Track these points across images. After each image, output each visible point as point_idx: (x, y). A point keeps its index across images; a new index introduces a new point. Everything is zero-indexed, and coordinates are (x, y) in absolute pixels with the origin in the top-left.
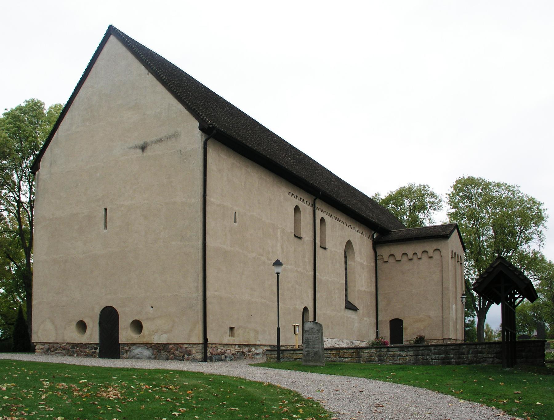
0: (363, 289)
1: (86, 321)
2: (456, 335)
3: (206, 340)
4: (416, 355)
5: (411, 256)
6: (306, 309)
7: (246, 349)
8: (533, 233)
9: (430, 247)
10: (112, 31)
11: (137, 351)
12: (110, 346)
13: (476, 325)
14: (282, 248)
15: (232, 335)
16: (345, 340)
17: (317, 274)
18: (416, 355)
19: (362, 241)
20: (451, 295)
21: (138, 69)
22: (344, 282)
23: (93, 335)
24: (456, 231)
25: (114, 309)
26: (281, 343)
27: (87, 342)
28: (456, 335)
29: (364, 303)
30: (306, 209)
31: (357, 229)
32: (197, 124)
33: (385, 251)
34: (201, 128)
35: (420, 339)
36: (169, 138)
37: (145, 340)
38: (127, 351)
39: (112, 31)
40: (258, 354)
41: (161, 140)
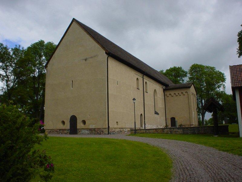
0: (160, 106)
1: (65, 121)
2: (195, 123)
3: (109, 127)
4: (183, 131)
5: (177, 94)
6: (141, 115)
7: (122, 130)
8: (221, 85)
9: (184, 91)
10: (74, 20)
11: (83, 131)
12: (74, 130)
13: (201, 119)
14: (133, 93)
15: (117, 125)
16: (155, 126)
17: (145, 102)
18: (184, 131)
19: (159, 88)
20: (192, 108)
21: (87, 37)
22: (154, 104)
23: (67, 126)
24: (193, 85)
25: (76, 117)
26: (136, 127)
27: (65, 128)
28: (195, 123)
29: (161, 112)
30: (141, 79)
31: (157, 85)
32: (105, 52)
33: (168, 93)
34: (106, 53)
35: (181, 125)
36: (95, 56)
37: (87, 127)
38: (80, 131)
39: (74, 20)
40: (126, 131)
41: (92, 57)
